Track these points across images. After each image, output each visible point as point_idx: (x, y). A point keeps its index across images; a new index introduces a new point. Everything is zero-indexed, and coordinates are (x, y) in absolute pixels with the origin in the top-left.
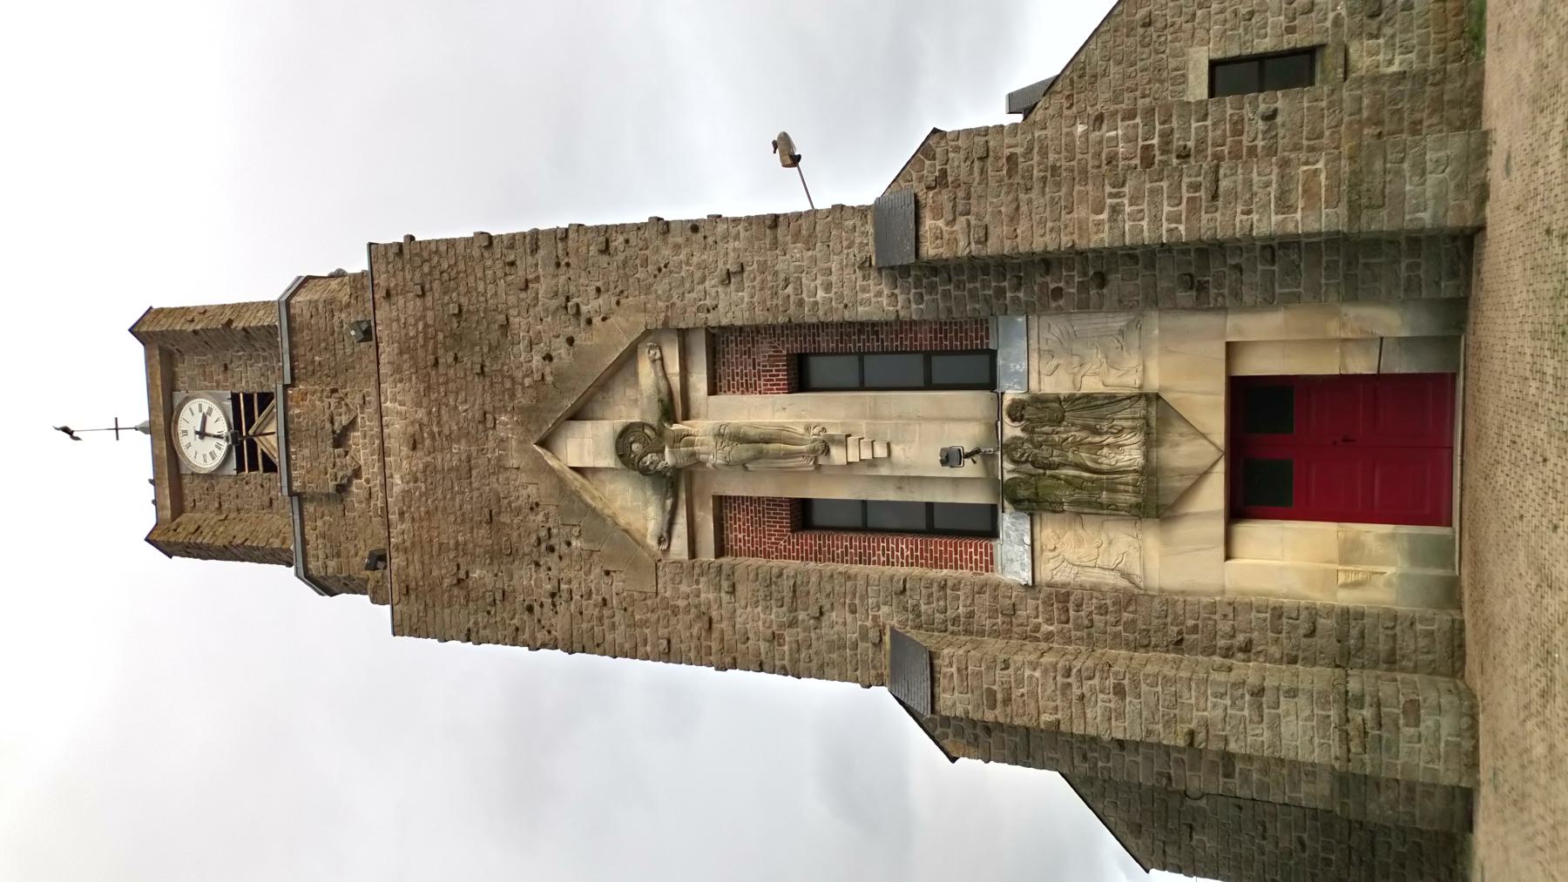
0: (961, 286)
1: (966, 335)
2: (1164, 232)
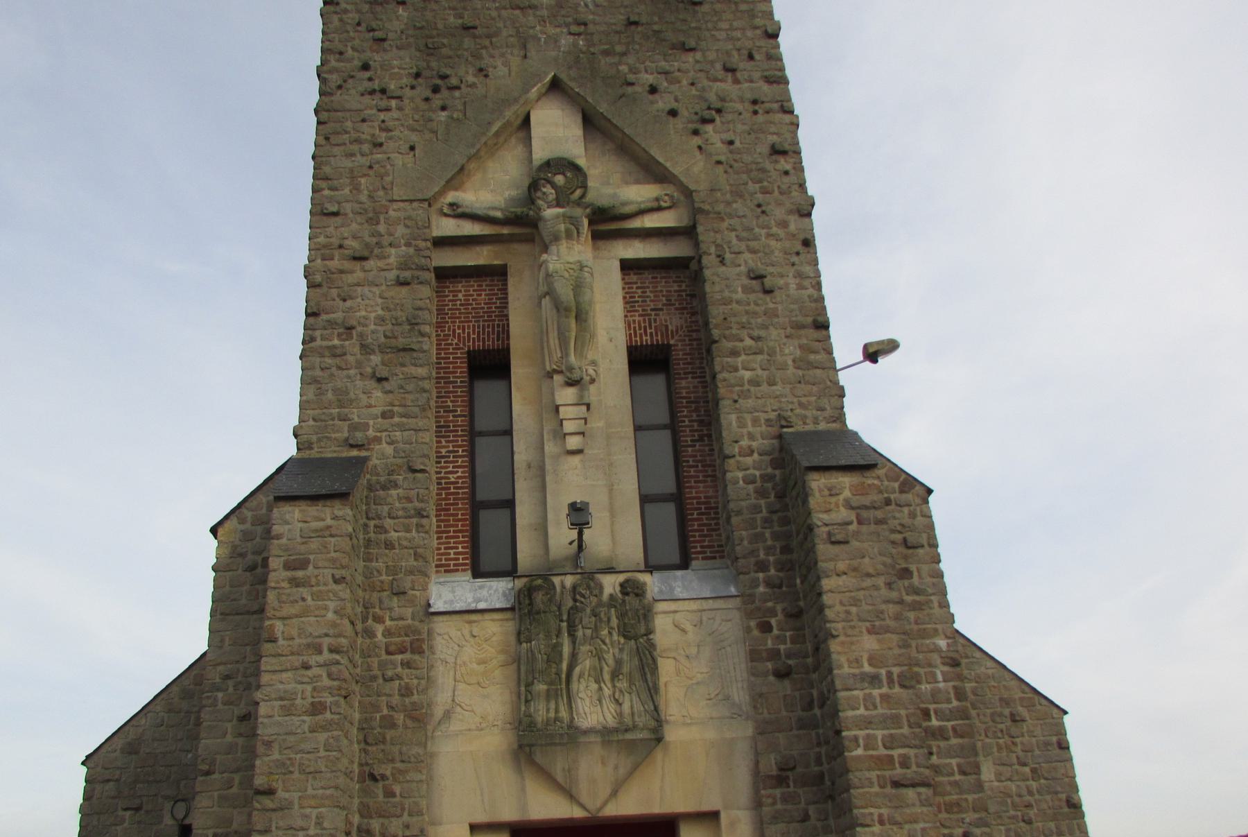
0: (766, 525)
1: (705, 536)
2: (853, 733)
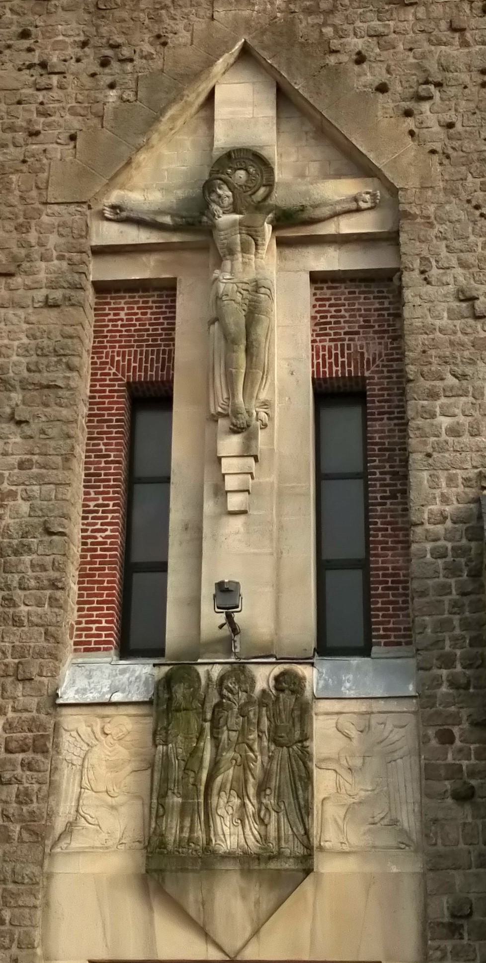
0: (456, 609)
1: (391, 616)
